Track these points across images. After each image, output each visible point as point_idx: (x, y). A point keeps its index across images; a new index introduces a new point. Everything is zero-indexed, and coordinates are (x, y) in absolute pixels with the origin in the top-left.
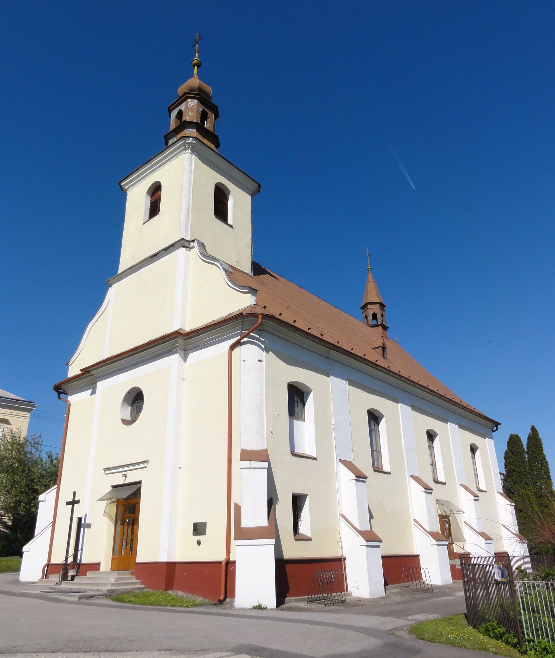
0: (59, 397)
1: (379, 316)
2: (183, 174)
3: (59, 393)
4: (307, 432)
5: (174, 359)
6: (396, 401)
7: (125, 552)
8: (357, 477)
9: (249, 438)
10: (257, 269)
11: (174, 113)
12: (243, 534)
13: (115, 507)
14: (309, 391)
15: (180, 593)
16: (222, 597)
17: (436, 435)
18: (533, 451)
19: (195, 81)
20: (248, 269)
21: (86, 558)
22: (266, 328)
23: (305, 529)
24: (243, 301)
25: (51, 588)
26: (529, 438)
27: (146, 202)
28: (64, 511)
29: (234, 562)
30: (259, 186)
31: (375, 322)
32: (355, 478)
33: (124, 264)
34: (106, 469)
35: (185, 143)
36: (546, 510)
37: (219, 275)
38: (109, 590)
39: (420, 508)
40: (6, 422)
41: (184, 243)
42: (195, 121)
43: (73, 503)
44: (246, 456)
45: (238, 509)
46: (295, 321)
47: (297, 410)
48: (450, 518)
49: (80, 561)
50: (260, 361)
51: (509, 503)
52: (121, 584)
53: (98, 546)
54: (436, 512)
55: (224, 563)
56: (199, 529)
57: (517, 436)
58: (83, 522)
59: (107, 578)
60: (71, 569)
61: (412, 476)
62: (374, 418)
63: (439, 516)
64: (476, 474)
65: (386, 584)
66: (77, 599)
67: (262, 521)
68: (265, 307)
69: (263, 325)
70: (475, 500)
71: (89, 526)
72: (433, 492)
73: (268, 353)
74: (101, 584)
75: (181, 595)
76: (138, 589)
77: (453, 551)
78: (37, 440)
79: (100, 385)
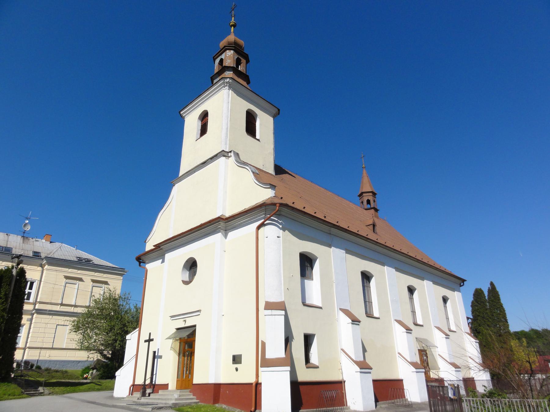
0: (140, 265)
1: (372, 202)
2: (223, 104)
3: (140, 263)
4: (314, 288)
5: (219, 236)
6: (383, 264)
7: (186, 376)
8: (352, 321)
9: (271, 292)
10: (279, 170)
11: (217, 61)
12: (265, 362)
13: (179, 344)
14: (316, 259)
15: (224, 406)
16: (253, 409)
17: (415, 289)
18: (492, 301)
19: (231, 38)
20: (271, 171)
21: (159, 381)
22: (283, 213)
23: (314, 359)
24: (266, 194)
25: (134, 402)
26: (489, 291)
27: (198, 125)
28: (144, 346)
29: (261, 384)
30: (279, 110)
31: (369, 206)
32: (351, 321)
33: (184, 168)
34: (172, 317)
35: (224, 82)
36: (505, 346)
37: (248, 175)
38: (173, 404)
39: (403, 345)
40: (106, 283)
41: (224, 154)
42: (232, 66)
43: (149, 341)
44: (270, 306)
45: (264, 344)
46: (304, 208)
47: (308, 272)
48: (427, 352)
49: (155, 383)
50: (278, 237)
51: (474, 340)
52: (182, 399)
53: (167, 372)
54: (416, 347)
55: (254, 384)
56: (237, 359)
57: (481, 290)
58: (156, 354)
59: (173, 395)
60: (148, 388)
61: (396, 321)
62: (366, 277)
63: (419, 350)
64: (448, 319)
65: (377, 401)
66: (150, 409)
67: (281, 354)
68: (282, 198)
69: (280, 211)
70: (446, 338)
71: (161, 357)
72: (413, 332)
73: (284, 231)
74: (168, 399)
75: (225, 408)
76: (194, 403)
77: (430, 376)
78: (126, 296)
79: (168, 256)
